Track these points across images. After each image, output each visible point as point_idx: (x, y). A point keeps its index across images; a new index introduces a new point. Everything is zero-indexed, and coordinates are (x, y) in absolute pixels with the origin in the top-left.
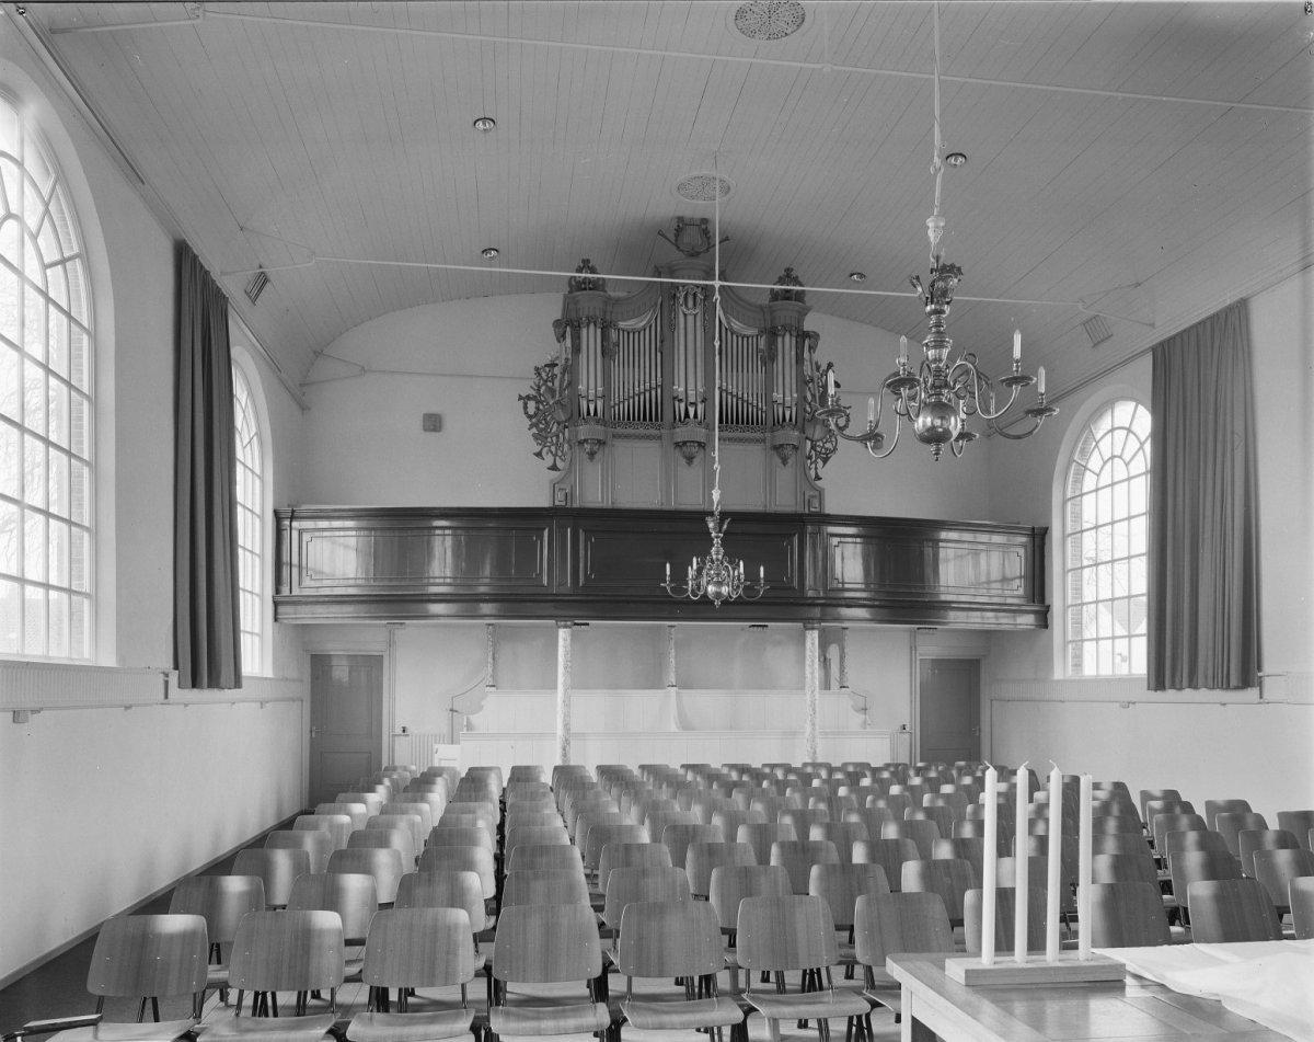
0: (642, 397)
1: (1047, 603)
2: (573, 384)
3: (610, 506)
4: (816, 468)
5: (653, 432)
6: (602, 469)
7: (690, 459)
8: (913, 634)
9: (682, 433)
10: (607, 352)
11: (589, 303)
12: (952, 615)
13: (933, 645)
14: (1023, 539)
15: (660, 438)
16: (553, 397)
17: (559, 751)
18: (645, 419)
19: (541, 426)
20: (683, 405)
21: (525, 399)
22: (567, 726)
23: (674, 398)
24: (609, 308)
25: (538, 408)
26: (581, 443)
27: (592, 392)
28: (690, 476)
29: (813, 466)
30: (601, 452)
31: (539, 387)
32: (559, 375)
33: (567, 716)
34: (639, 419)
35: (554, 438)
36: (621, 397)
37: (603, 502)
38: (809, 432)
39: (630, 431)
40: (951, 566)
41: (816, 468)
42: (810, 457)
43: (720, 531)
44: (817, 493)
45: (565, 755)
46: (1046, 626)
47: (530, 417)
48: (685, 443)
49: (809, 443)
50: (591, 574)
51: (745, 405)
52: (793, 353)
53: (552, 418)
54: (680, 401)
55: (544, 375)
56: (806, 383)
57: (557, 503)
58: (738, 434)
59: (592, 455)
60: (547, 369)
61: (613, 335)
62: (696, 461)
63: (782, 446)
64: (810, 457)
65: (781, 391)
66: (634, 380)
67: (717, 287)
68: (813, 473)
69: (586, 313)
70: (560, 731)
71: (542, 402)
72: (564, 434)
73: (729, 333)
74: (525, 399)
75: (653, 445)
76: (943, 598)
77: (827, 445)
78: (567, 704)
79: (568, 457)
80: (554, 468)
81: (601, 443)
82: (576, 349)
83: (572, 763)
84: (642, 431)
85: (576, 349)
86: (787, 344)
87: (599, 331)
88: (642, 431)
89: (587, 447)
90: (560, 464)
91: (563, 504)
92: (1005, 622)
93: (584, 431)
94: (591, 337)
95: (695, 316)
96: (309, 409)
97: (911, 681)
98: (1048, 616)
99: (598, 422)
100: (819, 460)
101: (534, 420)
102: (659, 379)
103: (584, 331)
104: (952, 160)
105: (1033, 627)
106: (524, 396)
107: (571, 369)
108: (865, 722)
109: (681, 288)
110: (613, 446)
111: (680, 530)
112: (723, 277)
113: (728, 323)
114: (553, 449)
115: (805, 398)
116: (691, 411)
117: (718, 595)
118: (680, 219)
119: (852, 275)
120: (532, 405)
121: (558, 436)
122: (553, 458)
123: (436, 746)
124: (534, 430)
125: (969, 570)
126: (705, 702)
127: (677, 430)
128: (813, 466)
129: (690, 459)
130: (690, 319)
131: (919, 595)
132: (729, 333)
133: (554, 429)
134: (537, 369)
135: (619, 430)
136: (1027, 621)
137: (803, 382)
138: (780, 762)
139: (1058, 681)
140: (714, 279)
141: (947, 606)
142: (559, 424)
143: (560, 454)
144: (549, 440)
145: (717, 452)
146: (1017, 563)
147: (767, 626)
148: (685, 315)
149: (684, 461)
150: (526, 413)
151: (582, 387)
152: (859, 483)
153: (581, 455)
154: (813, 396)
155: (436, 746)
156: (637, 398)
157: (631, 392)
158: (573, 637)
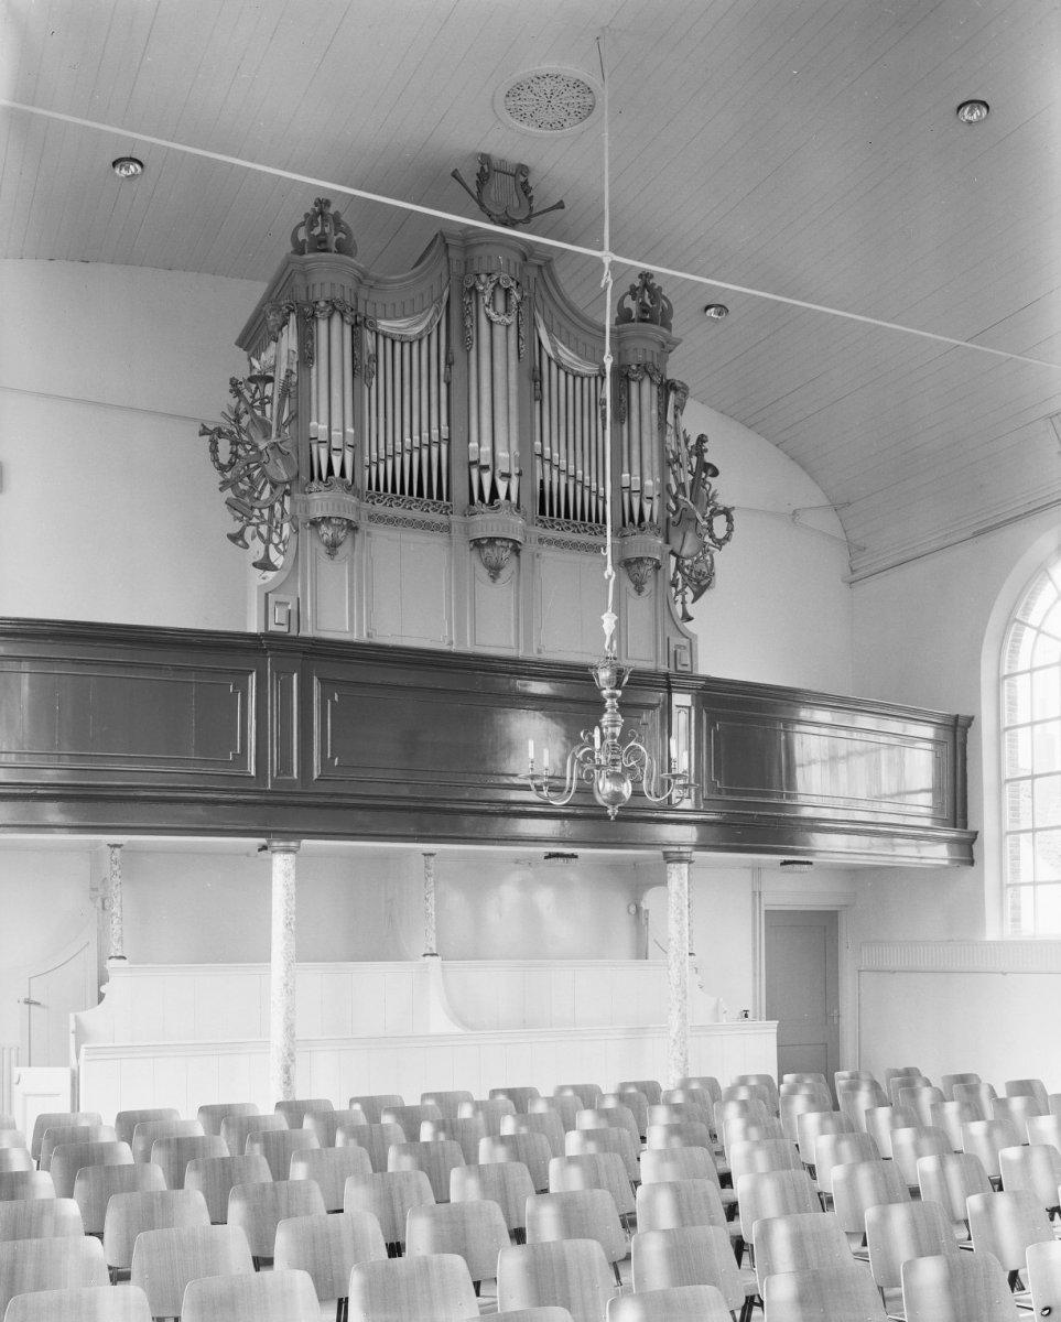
0: (416, 455)
1: (972, 827)
2: (299, 417)
3: (364, 639)
4: (683, 603)
5: (438, 518)
6: (351, 573)
7: (495, 570)
8: (757, 869)
9: (487, 523)
10: (362, 369)
11: (328, 277)
12: (820, 841)
13: (790, 889)
14: (928, 732)
15: (448, 528)
16: (266, 436)
17: (276, 1074)
18: (420, 494)
19: (241, 486)
20: (487, 477)
21: (213, 434)
22: (290, 1029)
23: (471, 464)
24: (363, 293)
25: (235, 454)
26: (315, 524)
27: (336, 435)
28: (496, 598)
29: (679, 598)
30: (349, 539)
31: (237, 420)
32: (276, 399)
33: (290, 1011)
34: (411, 493)
35: (266, 512)
36: (382, 451)
37: (351, 630)
38: (676, 543)
39: (397, 511)
40: (816, 770)
41: (683, 603)
42: (674, 584)
43: (618, 687)
44: (685, 642)
45: (288, 1082)
46: (972, 863)
47: (222, 468)
48: (492, 540)
49: (673, 559)
50: (333, 758)
51: (579, 488)
52: (654, 412)
53: (263, 474)
54: (486, 468)
55: (247, 394)
56: (670, 464)
57: (272, 627)
58: (568, 536)
59: (333, 547)
60: (253, 386)
61: (369, 339)
62: (504, 573)
63: (640, 560)
64: (674, 584)
65: (636, 470)
66: (406, 430)
67: (607, 261)
68: (679, 609)
69: (327, 295)
70: (277, 1037)
71: (243, 443)
72: (282, 503)
73: (554, 366)
74: (213, 434)
75: (436, 541)
76: (807, 812)
77: (698, 567)
78: (290, 990)
79: (291, 547)
80: (265, 565)
81: (352, 528)
82: (306, 357)
83: (299, 1098)
84: (417, 514)
85: (306, 357)
86: (644, 395)
87: (348, 330)
88: (417, 514)
89: (327, 532)
90: (276, 558)
91: (284, 629)
92: (906, 853)
93: (322, 502)
94: (333, 337)
95: (508, 326)
96: (484, 156)
97: (754, 949)
98: (975, 847)
99: (348, 488)
100: (688, 589)
101: (228, 475)
102: (444, 428)
103: (323, 325)
104: (966, 114)
105: (946, 862)
106: (211, 427)
107: (295, 393)
108: (716, 1009)
109: (483, 277)
110: (369, 534)
111: (469, 687)
112: (614, 250)
113: (555, 349)
114: (264, 529)
115: (668, 487)
116: (502, 487)
117: (617, 796)
118: (485, 159)
119: (708, 308)
120: (224, 446)
121: (272, 508)
122: (263, 546)
123: (17, 1071)
124: (229, 493)
125: (855, 774)
126: (492, 984)
127: (478, 518)
128: (679, 598)
129: (495, 570)
130: (499, 330)
131: (781, 807)
132: (554, 366)
133: (266, 494)
134: (234, 383)
135: (379, 508)
136: (939, 854)
137: (669, 463)
138: (632, 1080)
139: (989, 943)
140: (601, 249)
141: (816, 826)
142: (275, 485)
143: (276, 539)
144: (256, 512)
145: (609, 549)
146: (921, 765)
147: (574, 856)
148: (491, 323)
149: (483, 573)
150: (216, 460)
151: (319, 427)
152: (731, 641)
153: (313, 545)
154: (681, 486)
155: (17, 1071)
156: (407, 456)
157: (398, 444)
158: (301, 874)
